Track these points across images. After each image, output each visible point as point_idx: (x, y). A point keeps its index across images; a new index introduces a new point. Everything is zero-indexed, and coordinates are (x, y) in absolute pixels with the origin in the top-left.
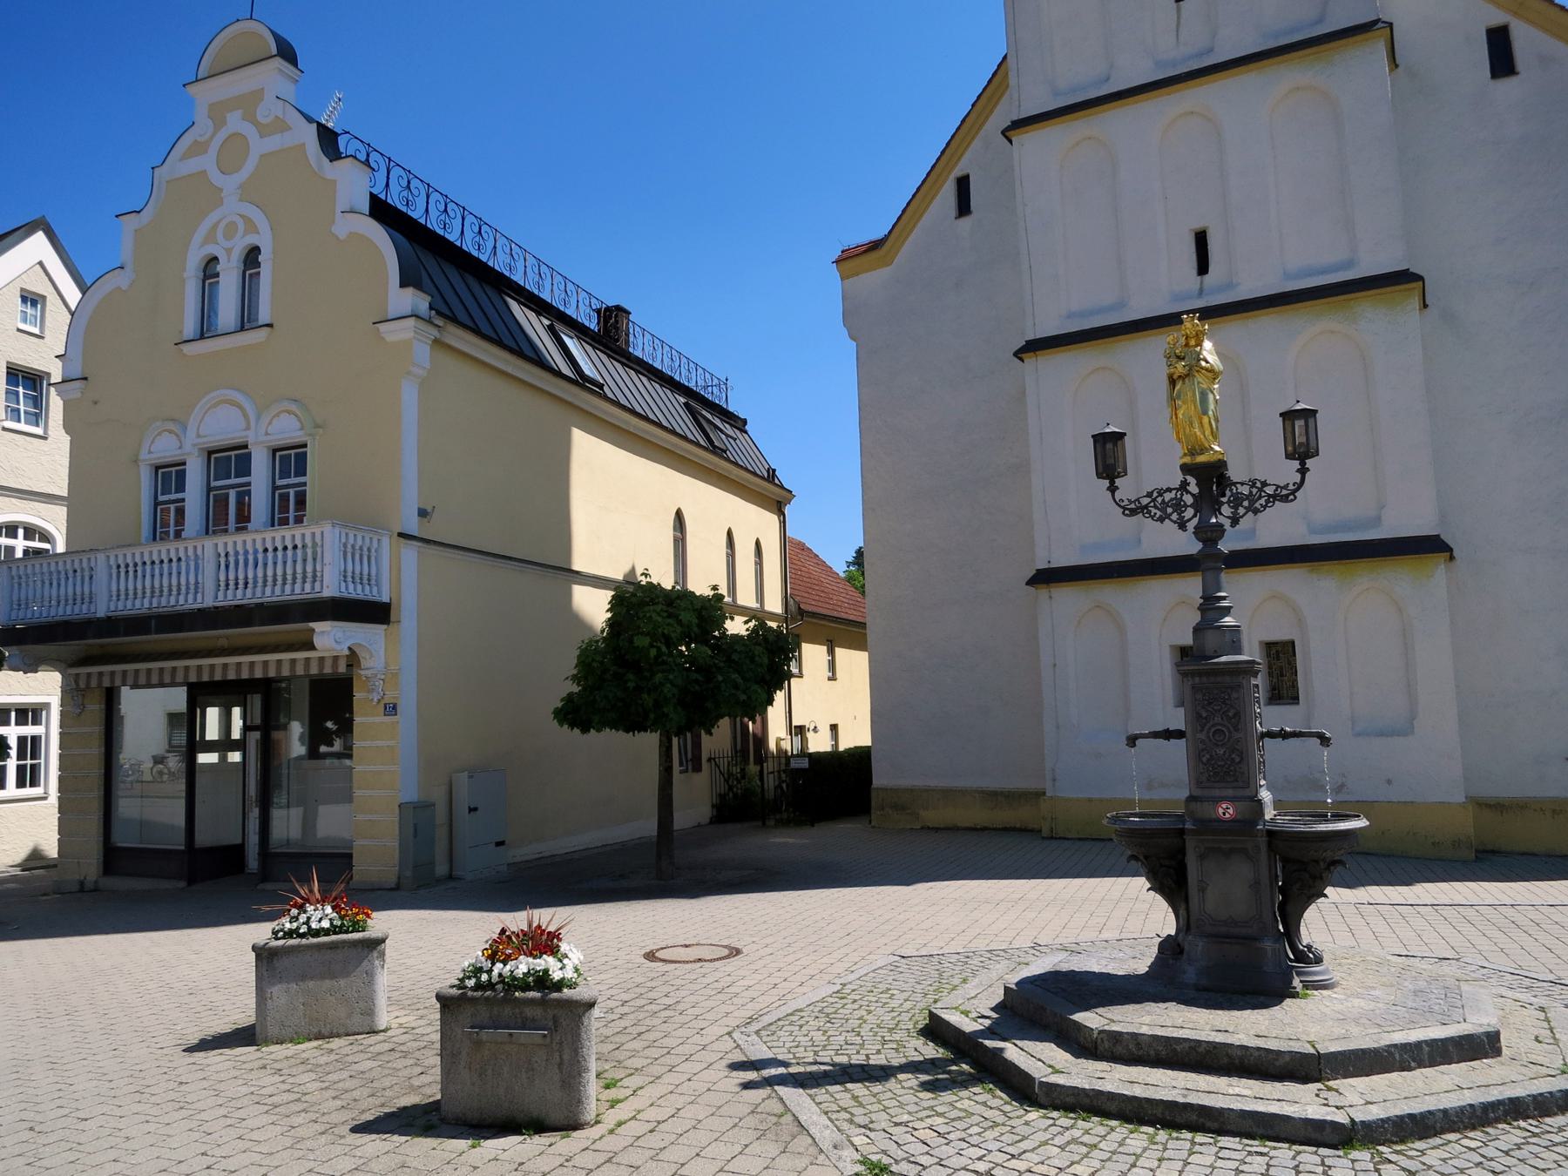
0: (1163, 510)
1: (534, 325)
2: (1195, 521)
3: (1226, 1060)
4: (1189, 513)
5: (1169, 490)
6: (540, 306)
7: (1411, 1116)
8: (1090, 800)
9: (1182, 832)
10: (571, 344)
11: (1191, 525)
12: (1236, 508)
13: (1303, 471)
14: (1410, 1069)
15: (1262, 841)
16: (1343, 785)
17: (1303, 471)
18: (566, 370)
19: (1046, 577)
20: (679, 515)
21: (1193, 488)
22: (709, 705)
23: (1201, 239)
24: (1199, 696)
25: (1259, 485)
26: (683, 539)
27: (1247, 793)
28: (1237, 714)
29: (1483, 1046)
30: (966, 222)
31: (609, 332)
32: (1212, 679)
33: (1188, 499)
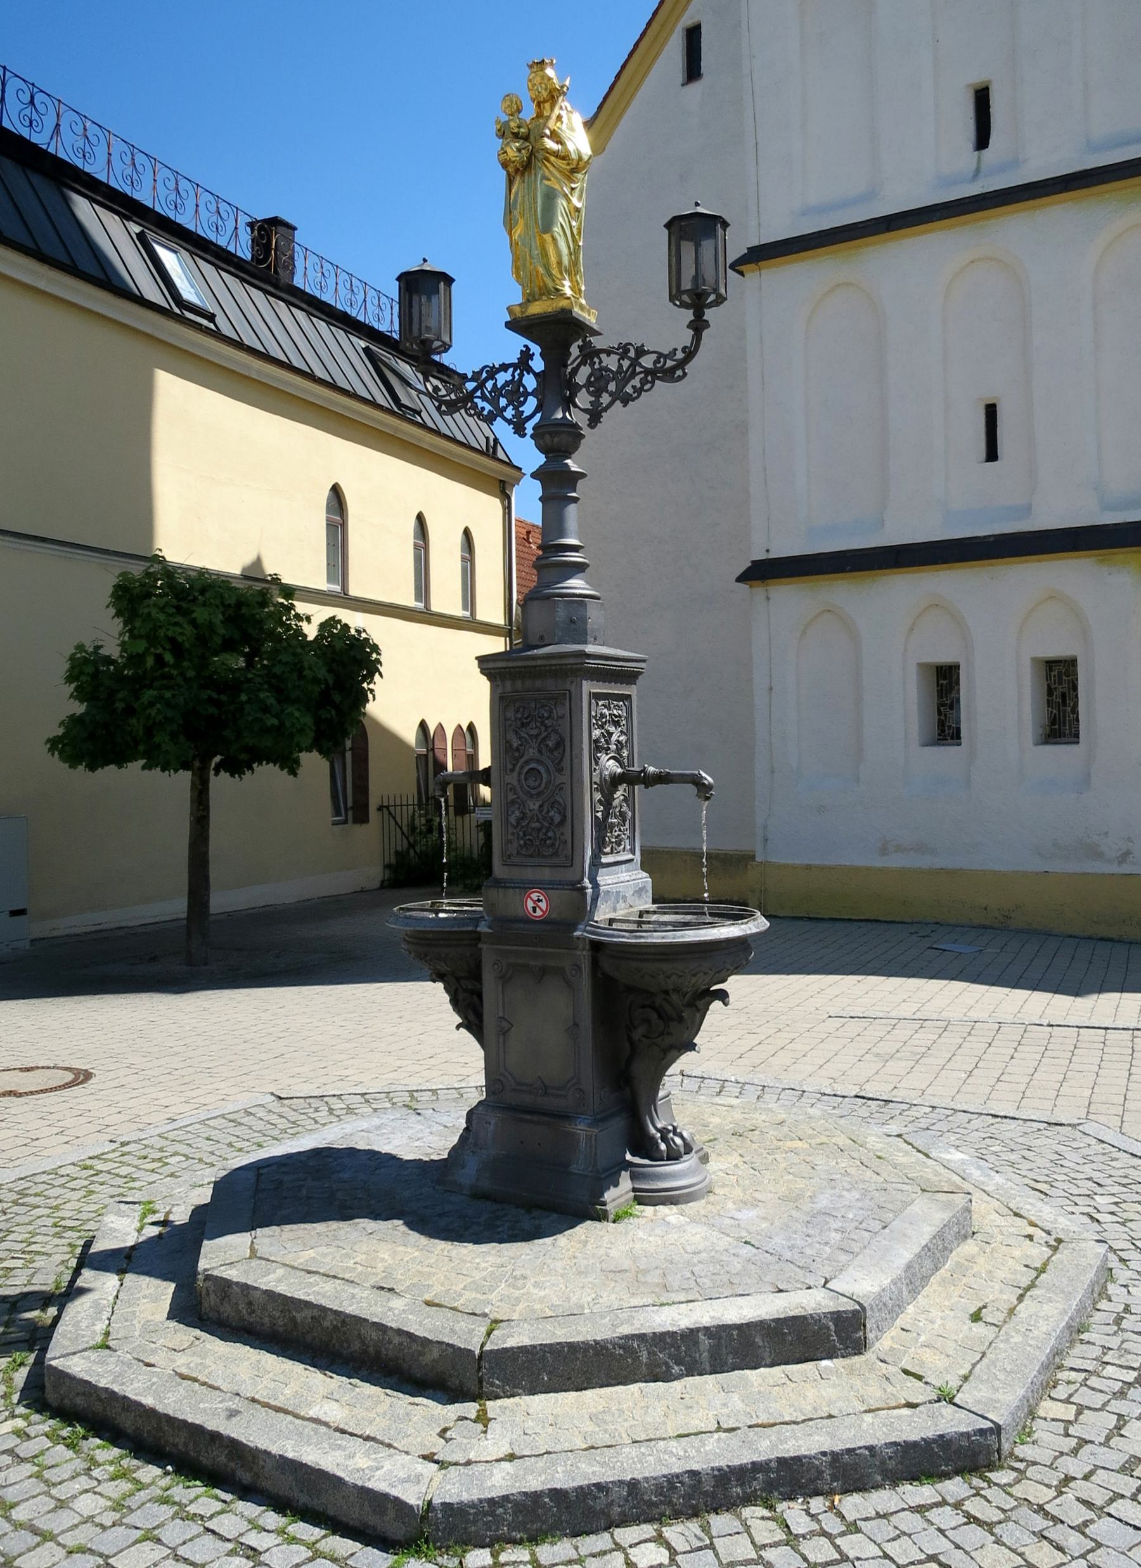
0: (494, 402)
1: (112, 235)
2: (537, 418)
3: (356, 1346)
4: (531, 404)
5: (504, 367)
6: (127, 207)
7: (557, 1494)
8: (809, 867)
9: (477, 937)
10: (169, 259)
11: (529, 426)
12: (597, 394)
13: (698, 326)
14: (667, 1378)
15: (584, 956)
16: (1128, 853)
17: (698, 326)
18: (152, 292)
19: (763, 572)
20: (336, 490)
21: (538, 364)
22: (227, 733)
23: (982, 99)
24: (510, 714)
25: (630, 352)
26: (344, 525)
27: (569, 875)
28: (560, 743)
29: (838, 1335)
30: (696, 87)
31: (266, 259)
32: (529, 683)
33: (530, 382)
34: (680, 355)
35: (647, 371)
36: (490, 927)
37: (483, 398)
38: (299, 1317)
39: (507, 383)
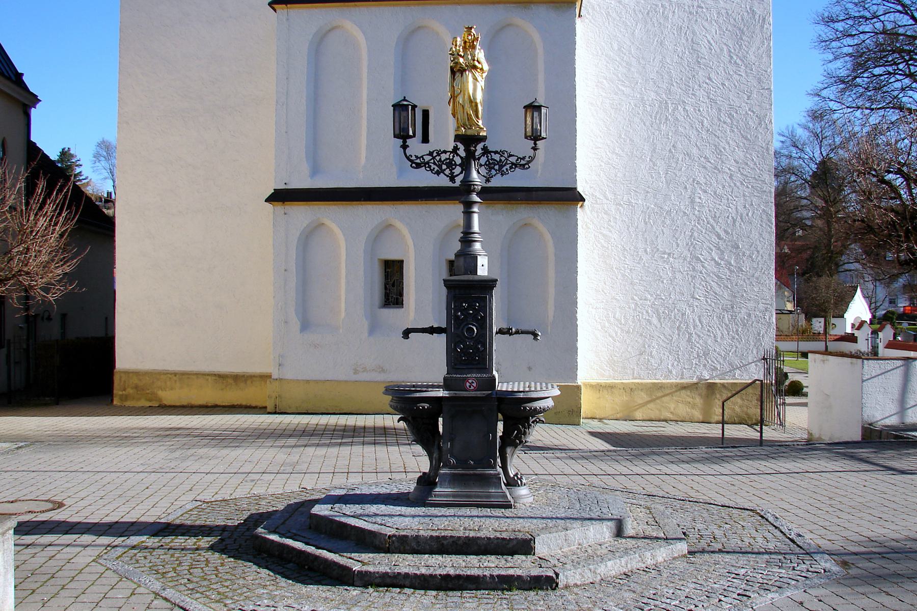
0: (440, 167)
4: (458, 170)
33: (458, 160)
34: (527, 159)
35: (512, 164)
36: (65, 261)
37: (434, 163)
38: (445, 542)
39: (447, 159)
